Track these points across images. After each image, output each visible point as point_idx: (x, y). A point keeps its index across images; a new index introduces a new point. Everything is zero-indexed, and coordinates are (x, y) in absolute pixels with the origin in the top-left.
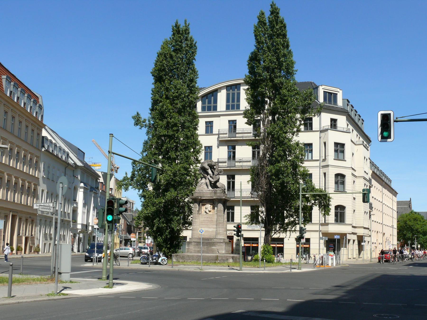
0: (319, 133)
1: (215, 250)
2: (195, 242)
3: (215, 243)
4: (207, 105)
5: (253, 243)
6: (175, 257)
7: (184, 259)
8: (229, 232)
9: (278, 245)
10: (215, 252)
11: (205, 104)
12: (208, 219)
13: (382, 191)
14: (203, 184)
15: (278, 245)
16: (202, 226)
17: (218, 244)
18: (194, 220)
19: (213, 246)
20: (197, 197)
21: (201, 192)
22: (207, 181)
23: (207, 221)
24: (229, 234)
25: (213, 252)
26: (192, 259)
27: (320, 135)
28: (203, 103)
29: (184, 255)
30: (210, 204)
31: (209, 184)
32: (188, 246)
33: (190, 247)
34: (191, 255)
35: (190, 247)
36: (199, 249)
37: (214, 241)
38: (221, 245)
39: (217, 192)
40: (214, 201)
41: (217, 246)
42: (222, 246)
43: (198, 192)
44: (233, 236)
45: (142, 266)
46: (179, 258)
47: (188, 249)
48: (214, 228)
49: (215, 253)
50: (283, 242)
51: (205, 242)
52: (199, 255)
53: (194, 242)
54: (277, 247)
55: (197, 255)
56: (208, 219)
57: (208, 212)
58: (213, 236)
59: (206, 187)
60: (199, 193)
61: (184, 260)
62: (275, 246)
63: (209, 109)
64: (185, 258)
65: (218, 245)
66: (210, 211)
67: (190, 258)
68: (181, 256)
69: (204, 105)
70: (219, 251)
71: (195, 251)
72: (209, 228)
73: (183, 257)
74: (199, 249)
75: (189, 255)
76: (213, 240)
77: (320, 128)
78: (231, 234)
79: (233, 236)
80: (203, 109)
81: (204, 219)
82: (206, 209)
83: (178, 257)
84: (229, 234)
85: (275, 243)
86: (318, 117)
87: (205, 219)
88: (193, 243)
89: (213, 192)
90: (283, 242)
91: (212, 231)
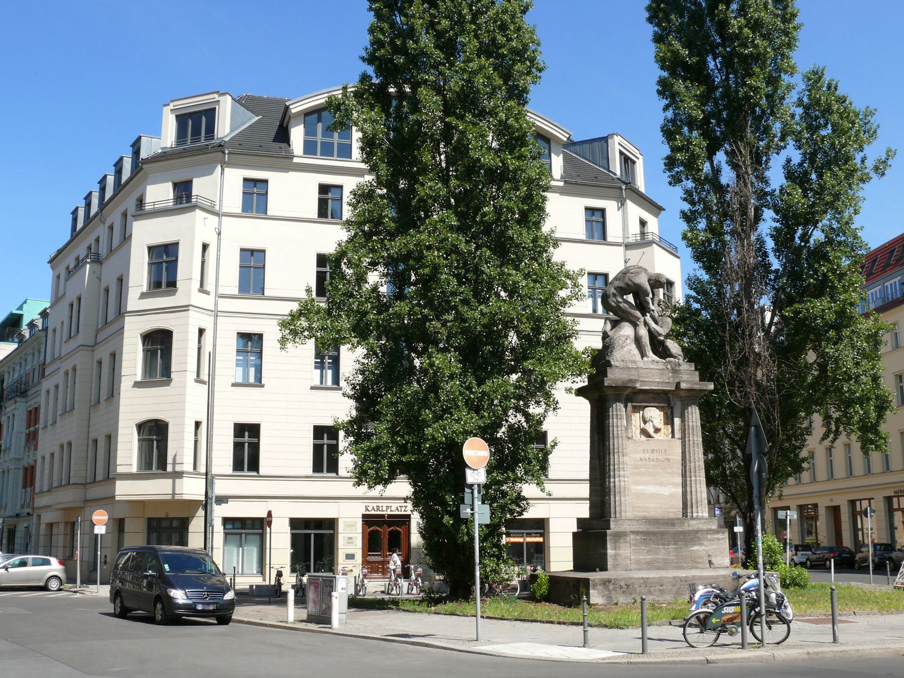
0: (622, 249)
1: (700, 557)
2: (637, 533)
3: (699, 535)
4: (319, 138)
5: (529, 535)
6: (601, 587)
7: (631, 594)
8: (399, 505)
9: (529, 539)
10: (702, 563)
11: (315, 135)
12: (655, 456)
13: (203, 418)
14: (628, 341)
15: (529, 539)
16: (638, 478)
17: (709, 536)
18: (621, 460)
19: (695, 545)
20: (631, 381)
21: (631, 366)
22: (643, 332)
23: (652, 463)
24: (397, 509)
25: (694, 563)
26: (660, 590)
27: (625, 255)
28: (309, 132)
29: (631, 579)
30: (657, 407)
31: (646, 340)
32: (615, 549)
33: (621, 552)
34: (654, 578)
35: (621, 552)
36: (651, 557)
37: (691, 528)
38: (719, 539)
39: (681, 368)
40: (671, 396)
41: (705, 543)
42: (722, 541)
43: (621, 364)
44: (409, 516)
45: (365, 632)
46: (615, 590)
47: (616, 556)
48: (675, 485)
49: (700, 566)
50: (542, 531)
51: (669, 532)
52: (680, 578)
53: (633, 532)
54: (528, 543)
55: (674, 578)
56: (655, 456)
57: (651, 430)
58: (674, 512)
59: (636, 352)
60: (623, 368)
61: (633, 596)
62: (521, 540)
63: (327, 151)
64: (635, 589)
65: (710, 540)
66: (657, 430)
67: (652, 589)
68: (622, 584)
69: (311, 138)
70: (714, 560)
71: (638, 562)
72: (661, 484)
73: (628, 586)
74: (651, 557)
75: (648, 578)
76: (686, 524)
77: (625, 236)
78: (403, 509)
79: (410, 515)
80: (309, 148)
81: (642, 456)
82: (645, 422)
83: (611, 587)
84: (397, 509)
85: (523, 533)
86: (619, 210)
87: (647, 456)
88: (632, 536)
89: (669, 367)
90: (542, 531)
91: (672, 496)
